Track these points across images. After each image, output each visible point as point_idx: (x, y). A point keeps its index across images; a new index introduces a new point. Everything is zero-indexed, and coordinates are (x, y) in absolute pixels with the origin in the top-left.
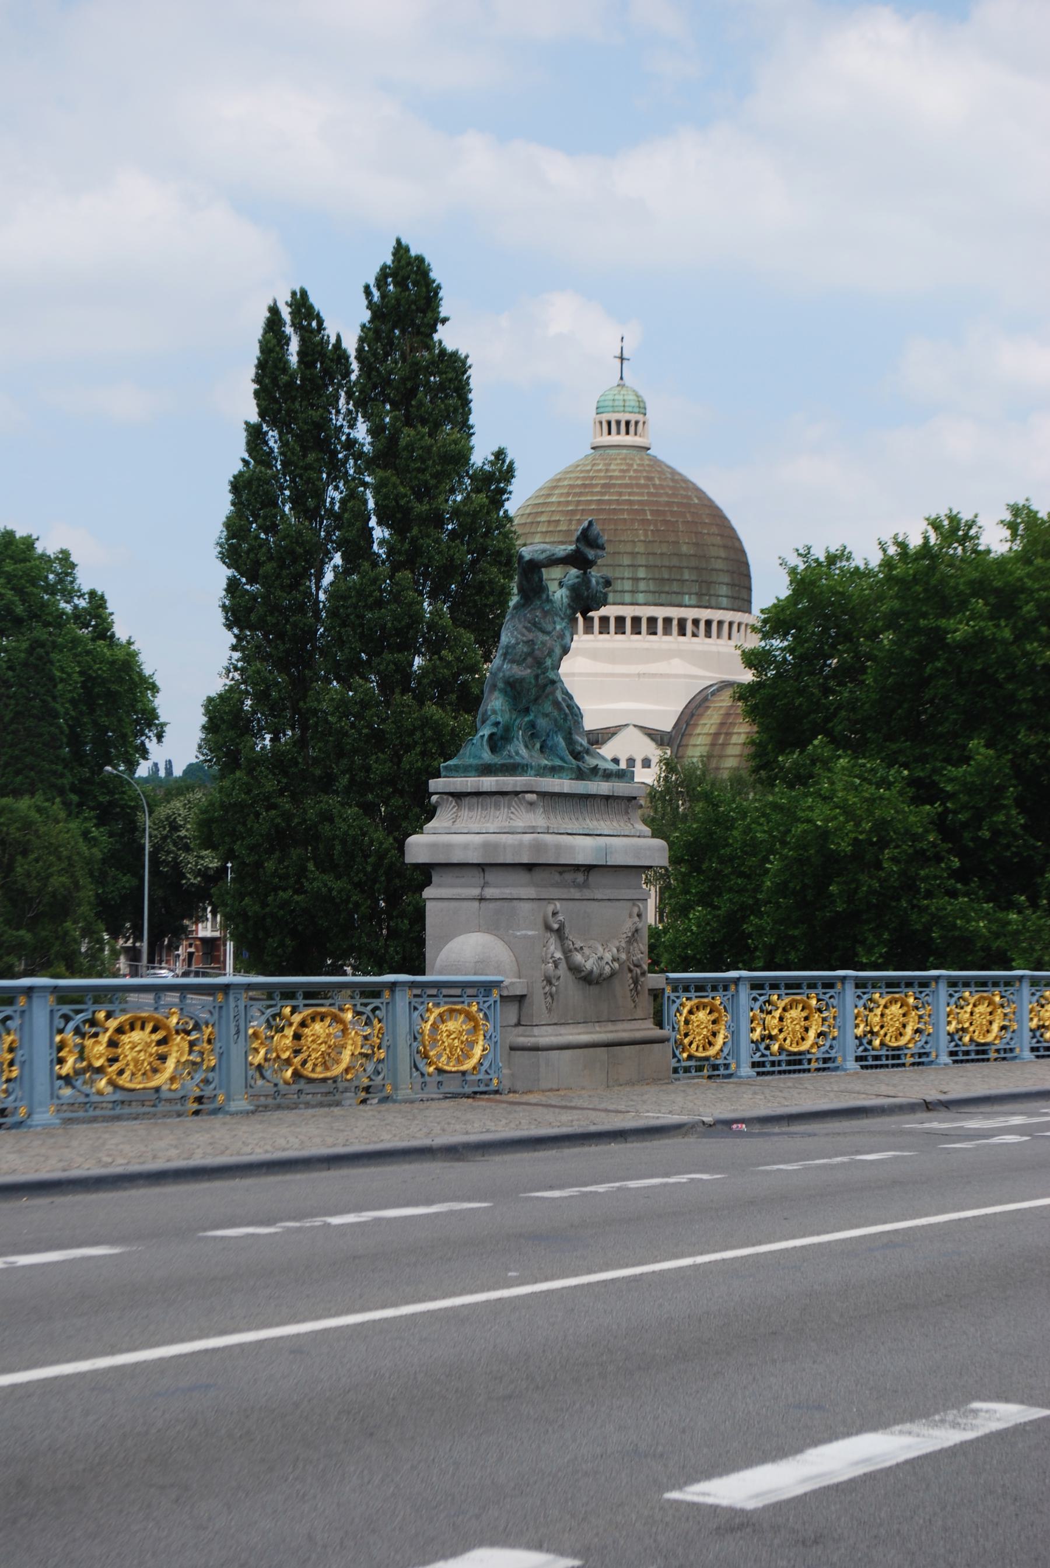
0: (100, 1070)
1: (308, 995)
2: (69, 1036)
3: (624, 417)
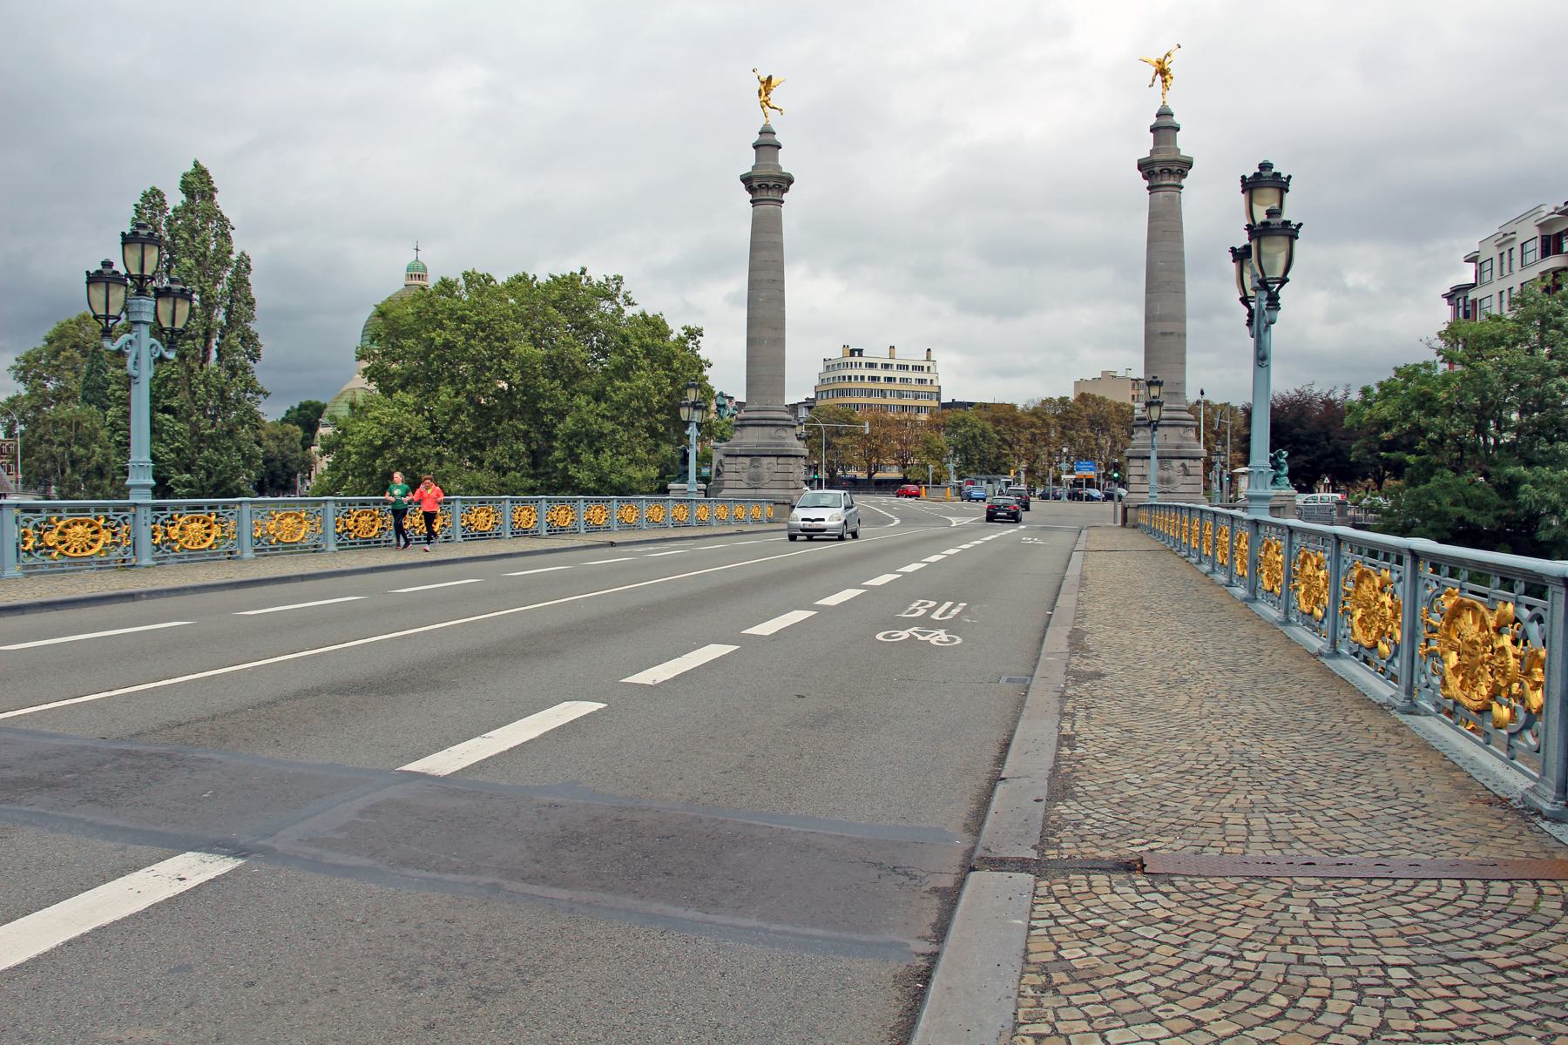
0: (54, 547)
1: (523, 502)
2: (158, 526)
3: (417, 273)
